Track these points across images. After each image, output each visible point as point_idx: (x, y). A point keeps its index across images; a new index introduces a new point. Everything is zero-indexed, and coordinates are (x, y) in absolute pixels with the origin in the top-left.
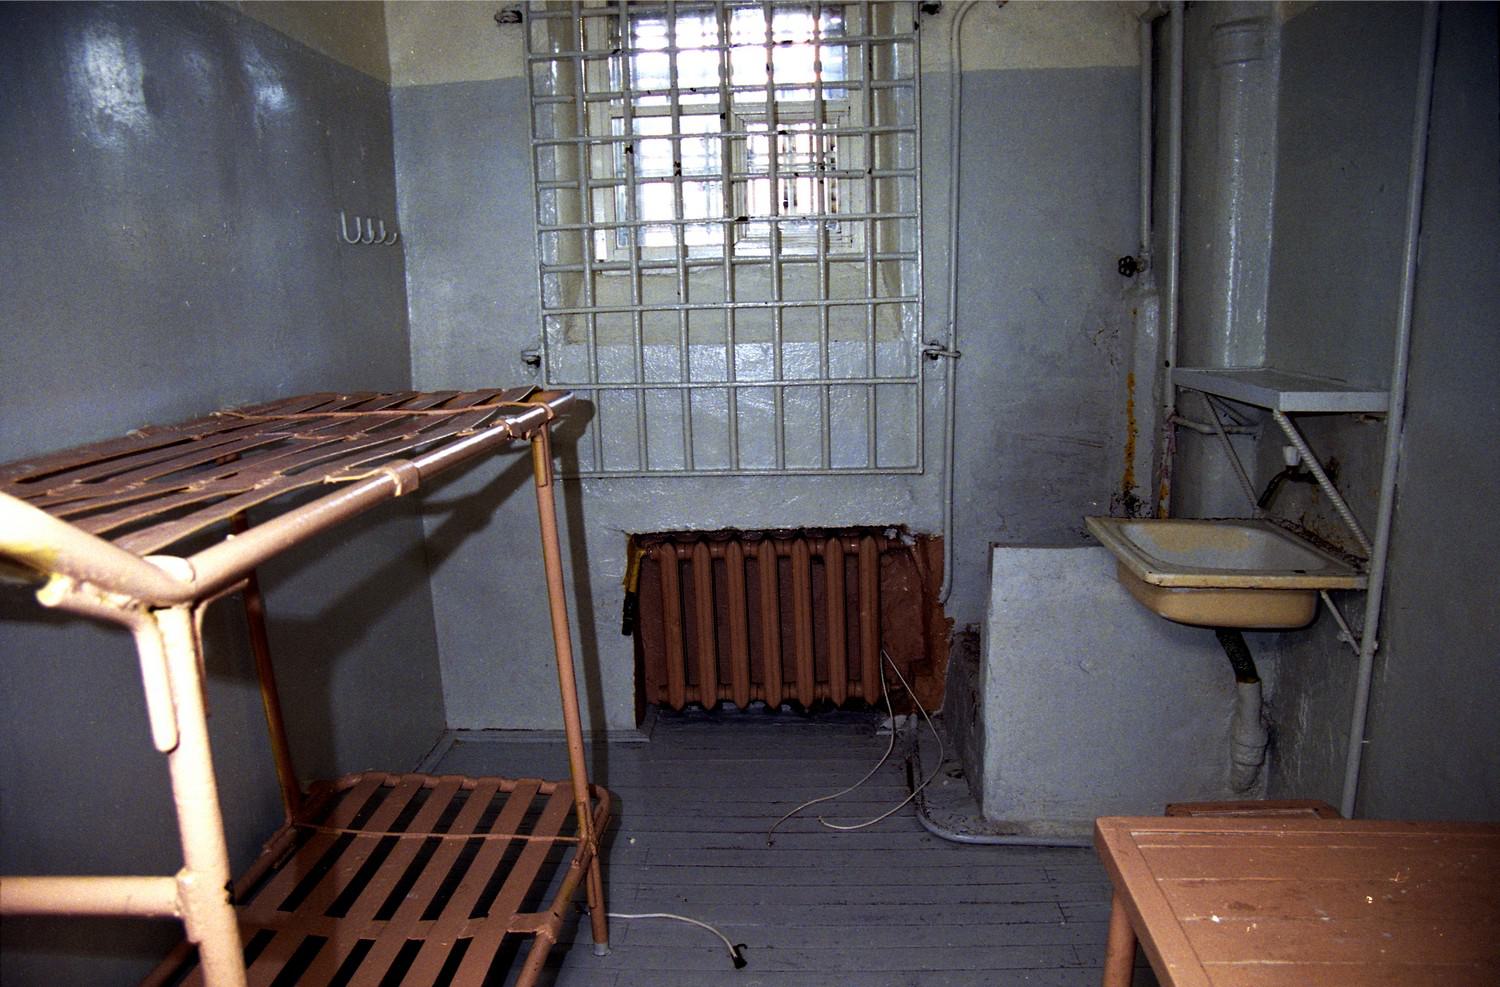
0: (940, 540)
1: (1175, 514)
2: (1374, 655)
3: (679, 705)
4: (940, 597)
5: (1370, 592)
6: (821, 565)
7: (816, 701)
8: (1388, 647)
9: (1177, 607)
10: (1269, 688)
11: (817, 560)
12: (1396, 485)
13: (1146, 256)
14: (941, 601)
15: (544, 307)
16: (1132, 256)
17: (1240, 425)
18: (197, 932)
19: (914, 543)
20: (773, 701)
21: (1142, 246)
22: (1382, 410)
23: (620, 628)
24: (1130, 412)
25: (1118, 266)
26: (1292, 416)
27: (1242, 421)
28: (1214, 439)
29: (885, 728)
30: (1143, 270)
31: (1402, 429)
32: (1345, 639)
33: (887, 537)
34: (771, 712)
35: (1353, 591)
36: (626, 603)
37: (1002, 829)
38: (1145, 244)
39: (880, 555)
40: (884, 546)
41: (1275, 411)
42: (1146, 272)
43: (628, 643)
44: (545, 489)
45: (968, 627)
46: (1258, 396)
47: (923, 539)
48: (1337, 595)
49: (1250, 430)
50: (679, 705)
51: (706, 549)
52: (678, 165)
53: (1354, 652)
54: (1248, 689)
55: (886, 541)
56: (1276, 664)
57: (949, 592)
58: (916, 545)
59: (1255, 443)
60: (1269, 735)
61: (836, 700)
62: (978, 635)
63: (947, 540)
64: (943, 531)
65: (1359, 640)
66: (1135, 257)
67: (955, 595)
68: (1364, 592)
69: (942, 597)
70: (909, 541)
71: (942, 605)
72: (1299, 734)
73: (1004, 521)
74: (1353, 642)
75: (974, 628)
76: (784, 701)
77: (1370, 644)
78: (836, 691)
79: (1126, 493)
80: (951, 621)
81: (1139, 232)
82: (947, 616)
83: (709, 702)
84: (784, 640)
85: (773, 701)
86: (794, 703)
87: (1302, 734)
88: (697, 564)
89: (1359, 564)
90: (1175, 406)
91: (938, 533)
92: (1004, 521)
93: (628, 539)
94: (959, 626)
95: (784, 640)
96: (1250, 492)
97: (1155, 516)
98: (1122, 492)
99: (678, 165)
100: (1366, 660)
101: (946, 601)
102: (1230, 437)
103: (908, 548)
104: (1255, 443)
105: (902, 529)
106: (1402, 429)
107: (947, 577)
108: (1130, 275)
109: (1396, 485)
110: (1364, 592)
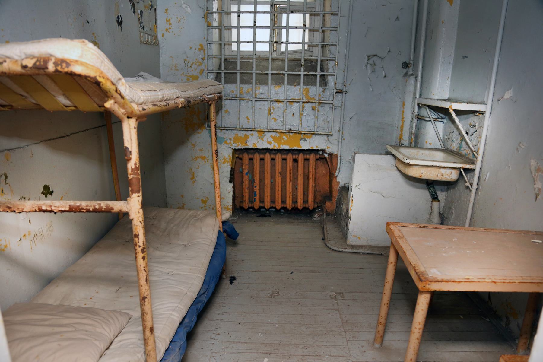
0: (336, 156)
1: (416, 146)
2: (476, 190)
3: (246, 208)
4: (336, 174)
5: (476, 170)
6: (296, 163)
7: (293, 208)
8: (481, 187)
9: (414, 172)
10: (442, 204)
11: (295, 161)
12: (487, 135)
13: (411, 62)
14: (336, 175)
15: (208, 70)
16: (407, 62)
17: (439, 118)
18: (132, 216)
19: (328, 156)
20: (278, 207)
21: (411, 59)
22: (484, 111)
23: (228, 181)
24: (403, 115)
25: (402, 66)
26: (455, 111)
27: (440, 117)
28: (430, 122)
29: (315, 217)
30: (410, 67)
31: (490, 116)
32: (467, 185)
33: (319, 154)
34: (277, 211)
35: (471, 169)
36: (231, 172)
37: (354, 247)
38: (412, 58)
39: (317, 160)
40: (318, 157)
41: (450, 109)
42: (411, 67)
43: (231, 185)
44: (213, 122)
45: (345, 185)
46: (446, 105)
47: (330, 155)
48: (466, 170)
49: (442, 120)
50: (246, 208)
51: (259, 156)
52: (255, 22)
53: (470, 189)
54: (436, 204)
55: (318, 155)
56: (445, 197)
57: (339, 173)
58: (328, 157)
59: (444, 124)
60: (442, 220)
61: (299, 208)
62: (348, 189)
63: (339, 155)
64: (338, 152)
65: (472, 186)
66: (408, 62)
67: (341, 174)
68: (474, 170)
69: (336, 174)
70: (326, 155)
71: (336, 177)
72: (451, 219)
73: (358, 150)
74: (470, 186)
75: (347, 185)
76: (282, 208)
77: (475, 186)
78: (300, 205)
79: (400, 142)
80: (339, 182)
81: (410, 55)
82: (338, 181)
83: (256, 207)
84: (284, 188)
85: (278, 207)
86: (284, 208)
87: (452, 219)
88: (255, 160)
89: (473, 163)
90: (418, 112)
91: (336, 153)
92: (358, 150)
93: (233, 150)
94: (341, 184)
95: (284, 188)
96: (441, 141)
97: (410, 147)
98: (398, 142)
99: (255, 22)
100: (474, 191)
101: (337, 176)
102: (435, 122)
103: (325, 158)
104: (444, 124)
105: (324, 151)
106: (490, 116)
107: (338, 167)
108: (406, 68)
109: (487, 135)
110: (474, 170)
